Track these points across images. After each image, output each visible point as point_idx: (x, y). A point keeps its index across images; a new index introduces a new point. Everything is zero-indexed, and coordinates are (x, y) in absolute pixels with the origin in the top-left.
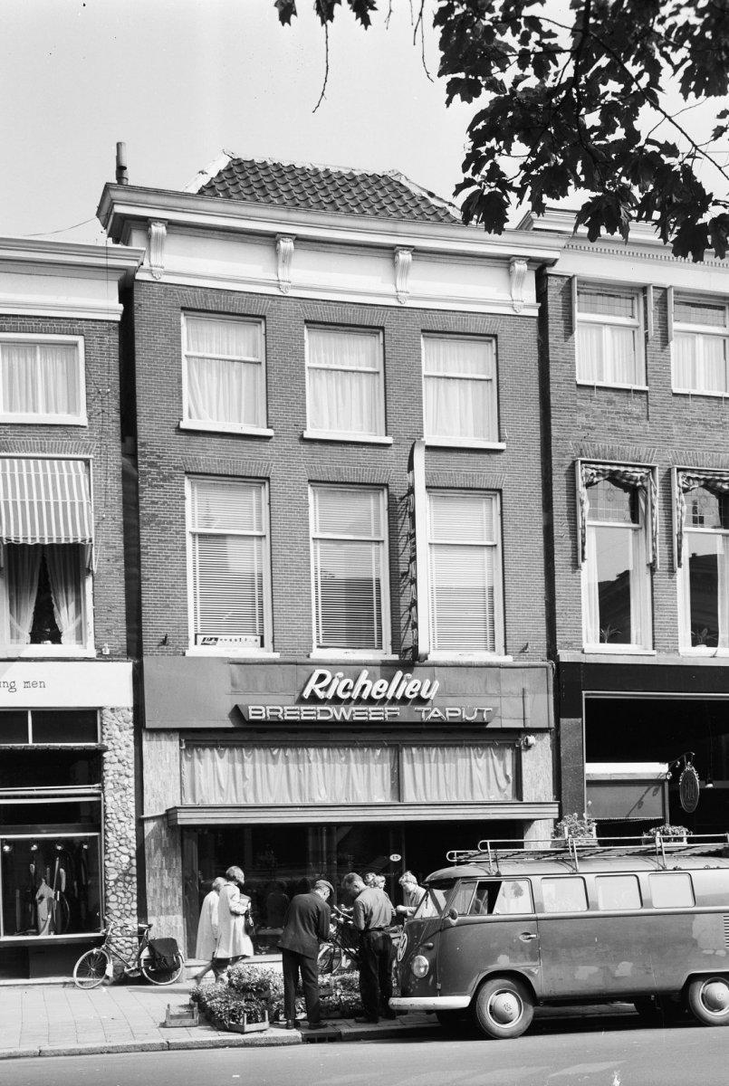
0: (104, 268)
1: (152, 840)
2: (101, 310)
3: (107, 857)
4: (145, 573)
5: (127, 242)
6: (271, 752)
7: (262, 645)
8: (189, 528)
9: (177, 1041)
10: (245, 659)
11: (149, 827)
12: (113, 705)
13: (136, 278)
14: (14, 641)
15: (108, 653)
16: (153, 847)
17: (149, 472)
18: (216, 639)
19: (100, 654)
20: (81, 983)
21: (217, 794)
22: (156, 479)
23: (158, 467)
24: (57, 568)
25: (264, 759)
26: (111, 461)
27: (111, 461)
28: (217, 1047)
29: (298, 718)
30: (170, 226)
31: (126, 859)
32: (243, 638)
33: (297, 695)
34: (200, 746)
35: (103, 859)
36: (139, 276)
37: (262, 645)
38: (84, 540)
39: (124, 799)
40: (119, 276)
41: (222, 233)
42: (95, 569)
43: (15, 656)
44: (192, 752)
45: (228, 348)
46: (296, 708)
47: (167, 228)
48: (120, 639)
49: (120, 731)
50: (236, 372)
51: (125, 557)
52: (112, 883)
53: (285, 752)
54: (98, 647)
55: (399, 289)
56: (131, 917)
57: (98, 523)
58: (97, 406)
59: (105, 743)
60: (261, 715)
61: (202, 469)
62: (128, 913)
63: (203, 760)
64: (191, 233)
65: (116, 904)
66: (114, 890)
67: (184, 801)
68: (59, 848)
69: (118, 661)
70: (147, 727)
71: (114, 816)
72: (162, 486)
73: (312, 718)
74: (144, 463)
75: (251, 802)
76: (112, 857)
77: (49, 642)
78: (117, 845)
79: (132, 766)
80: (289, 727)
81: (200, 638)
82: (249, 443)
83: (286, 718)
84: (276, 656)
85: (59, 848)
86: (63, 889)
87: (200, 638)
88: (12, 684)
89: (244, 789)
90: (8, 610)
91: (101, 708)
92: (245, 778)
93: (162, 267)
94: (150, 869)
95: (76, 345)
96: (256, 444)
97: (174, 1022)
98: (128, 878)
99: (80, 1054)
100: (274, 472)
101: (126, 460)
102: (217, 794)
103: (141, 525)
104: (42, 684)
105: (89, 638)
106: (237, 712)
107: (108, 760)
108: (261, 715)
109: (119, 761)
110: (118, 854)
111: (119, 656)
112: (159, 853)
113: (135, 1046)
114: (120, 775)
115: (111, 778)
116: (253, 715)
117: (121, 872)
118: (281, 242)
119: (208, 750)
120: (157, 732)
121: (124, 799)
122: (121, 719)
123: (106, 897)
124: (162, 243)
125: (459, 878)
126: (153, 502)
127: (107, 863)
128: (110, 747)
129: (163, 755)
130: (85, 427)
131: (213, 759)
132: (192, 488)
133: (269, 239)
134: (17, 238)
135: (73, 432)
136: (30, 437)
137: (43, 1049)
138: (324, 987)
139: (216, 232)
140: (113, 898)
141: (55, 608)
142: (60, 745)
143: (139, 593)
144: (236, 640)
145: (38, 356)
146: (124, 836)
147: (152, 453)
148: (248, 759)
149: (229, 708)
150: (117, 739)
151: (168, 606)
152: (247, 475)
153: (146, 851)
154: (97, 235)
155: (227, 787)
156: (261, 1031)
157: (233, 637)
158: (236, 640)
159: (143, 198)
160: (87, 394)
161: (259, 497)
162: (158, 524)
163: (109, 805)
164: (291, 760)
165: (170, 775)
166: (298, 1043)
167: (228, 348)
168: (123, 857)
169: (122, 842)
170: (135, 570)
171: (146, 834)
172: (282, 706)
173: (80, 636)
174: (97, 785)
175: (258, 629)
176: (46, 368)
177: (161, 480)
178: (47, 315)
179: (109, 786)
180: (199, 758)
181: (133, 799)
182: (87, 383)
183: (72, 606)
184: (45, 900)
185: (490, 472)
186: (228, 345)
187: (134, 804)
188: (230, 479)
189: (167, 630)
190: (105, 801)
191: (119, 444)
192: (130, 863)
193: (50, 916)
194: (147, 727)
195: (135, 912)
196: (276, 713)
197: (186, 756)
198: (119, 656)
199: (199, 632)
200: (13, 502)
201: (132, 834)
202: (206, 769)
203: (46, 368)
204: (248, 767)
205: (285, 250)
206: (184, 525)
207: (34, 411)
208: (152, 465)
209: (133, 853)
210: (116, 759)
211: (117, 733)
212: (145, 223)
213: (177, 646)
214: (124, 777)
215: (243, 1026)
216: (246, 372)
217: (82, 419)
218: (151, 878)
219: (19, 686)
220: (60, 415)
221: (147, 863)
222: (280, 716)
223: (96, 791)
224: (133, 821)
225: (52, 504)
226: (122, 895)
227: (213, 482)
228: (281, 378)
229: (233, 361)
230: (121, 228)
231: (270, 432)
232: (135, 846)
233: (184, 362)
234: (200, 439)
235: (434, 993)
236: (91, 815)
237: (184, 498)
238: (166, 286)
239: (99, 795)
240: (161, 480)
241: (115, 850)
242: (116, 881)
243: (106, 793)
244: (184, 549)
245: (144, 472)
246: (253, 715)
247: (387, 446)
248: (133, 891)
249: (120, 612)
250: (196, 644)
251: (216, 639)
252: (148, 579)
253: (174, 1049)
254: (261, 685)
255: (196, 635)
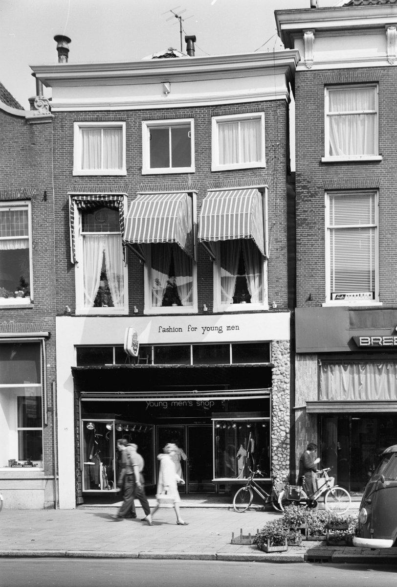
0: (273, 67)
1: (300, 422)
2: (276, 94)
3: (273, 432)
4: (299, 256)
5: (292, 47)
6: (378, 366)
7: (374, 298)
8: (327, 224)
9: (223, 554)
10: (359, 307)
11: (298, 414)
12: (278, 339)
13: (297, 70)
14: (224, 302)
15: (276, 307)
16: (300, 427)
17: (302, 192)
18: (344, 296)
19: (271, 308)
20: (237, 508)
21: (342, 394)
22: (306, 196)
23: (308, 189)
24: (231, 259)
25: (373, 371)
26: (279, 188)
27: (279, 188)
28: (247, 560)
29: (392, 344)
30: (317, 33)
31: (283, 434)
32: (361, 294)
33: (393, 329)
34: (332, 364)
35: (271, 433)
36: (298, 69)
37: (374, 298)
38: (246, 236)
39: (283, 397)
40: (285, 70)
41: (350, 31)
42: (268, 256)
43: (222, 311)
44: (327, 367)
45: (356, 106)
46: (392, 337)
47: (314, 34)
48: (283, 298)
49: (282, 355)
50: (361, 121)
51: (288, 246)
52: (275, 448)
53: (387, 366)
54: (270, 304)
55: (389, 54)
56: (286, 470)
57: (272, 227)
58: (272, 155)
59: (273, 362)
60: (368, 343)
61: (335, 186)
62: (284, 467)
63: (333, 372)
64: (331, 35)
65: (277, 461)
66: (276, 453)
67: (321, 398)
68: (249, 426)
69: (281, 312)
70: (297, 352)
71: (277, 407)
72: (310, 200)
73: (390, 344)
74: (299, 187)
75: (364, 398)
76: (276, 432)
77: (245, 302)
78: (278, 425)
79: (289, 376)
80: (387, 350)
81: (334, 296)
82: (367, 167)
83: (384, 344)
84: (380, 304)
85: (249, 426)
86: (252, 451)
87: (334, 296)
88: (220, 328)
89: (359, 391)
90: (220, 284)
91: (271, 341)
92: (360, 384)
93: (394, 56)
94: (298, 440)
95: (121, 128)
96: (370, 166)
97: (245, 541)
98: (284, 446)
99: (163, 558)
100: (383, 183)
101: (289, 186)
102: (342, 394)
103: (297, 226)
104: (237, 328)
105: (265, 299)
106: (353, 342)
107: (274, 373)
108: (368, 343)
109: (281, 374)
110: (279, 430)
111: (282, 309)
112: (304, 431)
113: (195, 556)
114: (282, 382)
115: (276, 384)
116: (362, 343)
117: (280, 442)
118: (388, 30)
119: (337, 366)
120: (305, 355)
121: (283, 397)
122: (283, 347)
123: (272, 457)
124: (312, 46)
125: (394, 453)
126: (305, 211)
127: (273, 436)
128: (276, 364)
129: (307, 369)
130: (264, 168)
131: (341, 372)
132: (331, 200)
133: (381, 29)
134: (241, 54)
135: (255, 171)
136: (232, 178)
137: (141, 554)
138: (342, 523)
139: (346, 31)
140: (275, 458)
141: (248, 281)
142: (260, 364)
143: (295, 269)
144: (363, 295)
145: (102, 135)
146: (282, 420)
147: (304, 180)
148: (362, 372)
149: (348, 339)
150: (280, 360)
151: (312, 276)
152: (364, 187)
153: (296, 429)
154: (278, 45)
155: (349, 390)
156: (280, 552)
157: (355, 294)
158: (357, 296)
159: (298, 16)
160: (266, 148)
161: (373, 202)
162: (307, 225)
163: (274, 400)
164: (390, 372)
165: (311, 382)
166: (301, 562)
167: (356, 106)
168: (282, 432)
169: (282, 423)
170: (293, 255)
171: (296, 419)
172: (382, 337)
173: (261, 299)
174: (269, 389)
175: (371, 288)
176: (244, 135)
177: (310, 196)
178: (83, 110)
179: (275, 389)
180: (332, 371)
181: (289, 397)
182: (266, 141)
183: (257, 279)
184: (242, 457)
185: (362, 177)
186: (356, 104)
187: (289, 400)
188: (355, 191)
189: (313, 291)
190: (272, 398)
191: (285, 177)
192: (286, 437)
193: (244, 467)
194: (297, 352)
195: (288, 467)
196: (377, 341)
197: (323, 370)
198: (282, 309)
199: (334, 292)
200: (157, 218)
201: (287, 419)
202: (335, 378)
203: (244, 135)
204: (362, 376)
205: (391, 35)
206: (323, 224)
207: (237, 162)
208: (304, 187)
209: (288, 430)
210: (279, 372)
211: (280, 357)
212: (300, 32)
213: (317, 301)
214: (283, 383)
215: (267, 548)
216: (367, 120)
217: (262, 164)
218: (299, 446)
219: (224, 329)
220: (91, 170)
221: (296, 436)
222: (380, 343)
223: (268, 392)
224: (289, 411)
225: (174, 219)
226: (281, 456)
227: (344, 195)
228: (388, 121)
229: (359, 114)
230: (289, 38)
231: (380, 158)
232: (289, 426)
233: (327, 120)
234: (334, 168)
235: (369, 536)
236: (264, 406)
237: (324, 207)
238: (314, 72)
239: (269, 394)
240: (310, 196)
241: (277, 428)
242: (278, 447)
243: (273, 393)
244: (323, 239)
245: (299, 192)
246: (362, 343)
247: (378, 162)
248: (287, 454)
249: (284, 280)
250: (331, 299)
251: (344, 296)
252: (301, 260)
253: (220, 560)
254: (369, 323)
255: (331, 294)
